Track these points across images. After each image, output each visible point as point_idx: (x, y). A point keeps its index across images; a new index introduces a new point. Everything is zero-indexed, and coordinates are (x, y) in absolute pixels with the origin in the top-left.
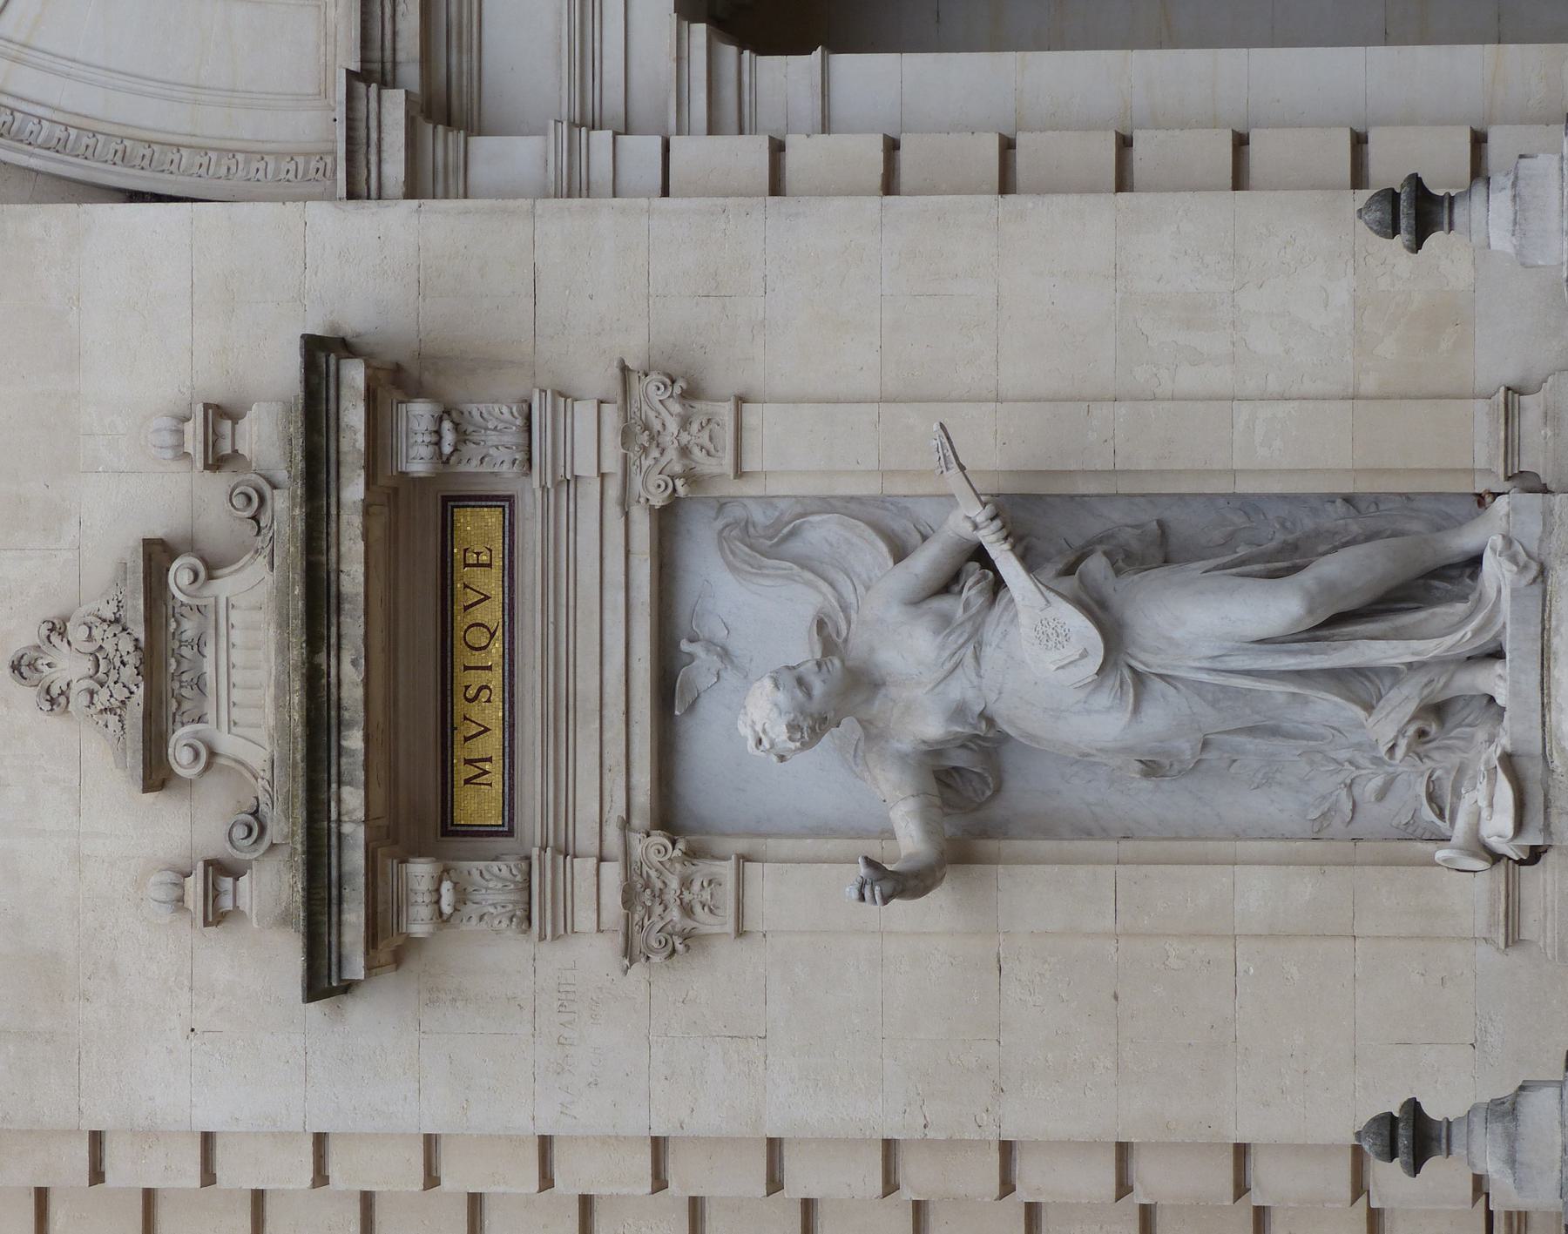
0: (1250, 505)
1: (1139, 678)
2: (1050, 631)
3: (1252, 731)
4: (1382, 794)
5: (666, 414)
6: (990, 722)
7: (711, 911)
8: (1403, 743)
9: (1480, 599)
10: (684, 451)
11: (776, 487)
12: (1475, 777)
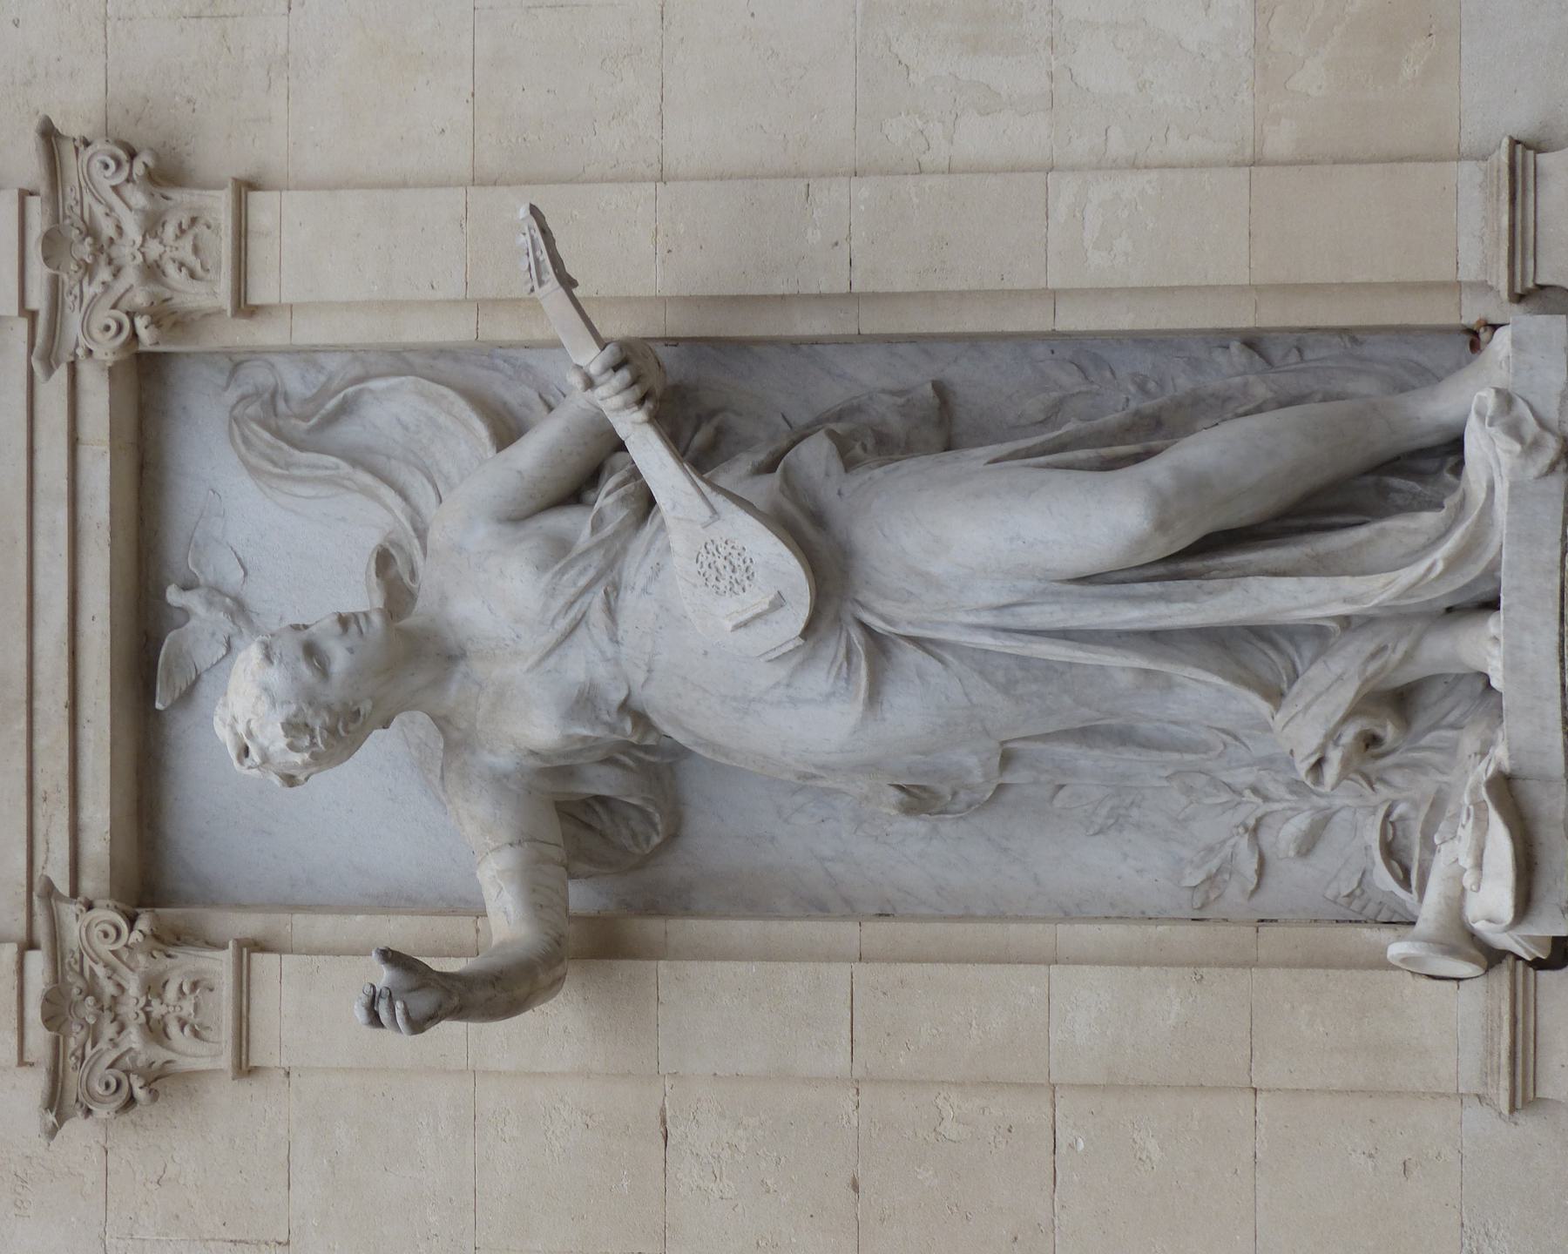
0: (1087, 351)
1: (878, 645)
2: (720, 563)
3: (1085, 735)
4: (1308, 845)
5: (122, 211)
6: (641, 719)
7: (196, 1034)
8: (1335, 756)
9: (1462, 506)
10: (152, 271)
11: (309, 332)
12: (1457, 816)
